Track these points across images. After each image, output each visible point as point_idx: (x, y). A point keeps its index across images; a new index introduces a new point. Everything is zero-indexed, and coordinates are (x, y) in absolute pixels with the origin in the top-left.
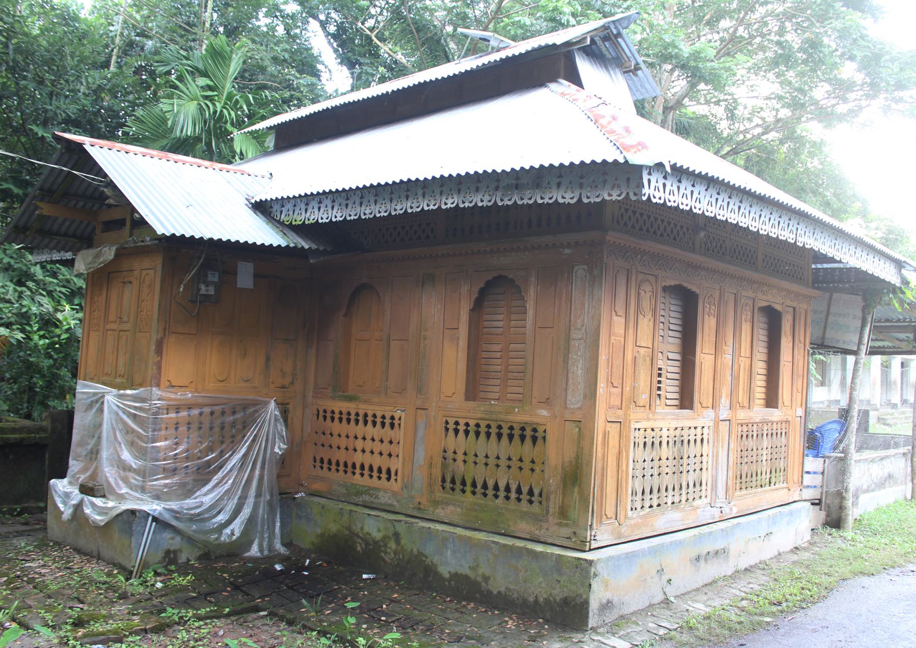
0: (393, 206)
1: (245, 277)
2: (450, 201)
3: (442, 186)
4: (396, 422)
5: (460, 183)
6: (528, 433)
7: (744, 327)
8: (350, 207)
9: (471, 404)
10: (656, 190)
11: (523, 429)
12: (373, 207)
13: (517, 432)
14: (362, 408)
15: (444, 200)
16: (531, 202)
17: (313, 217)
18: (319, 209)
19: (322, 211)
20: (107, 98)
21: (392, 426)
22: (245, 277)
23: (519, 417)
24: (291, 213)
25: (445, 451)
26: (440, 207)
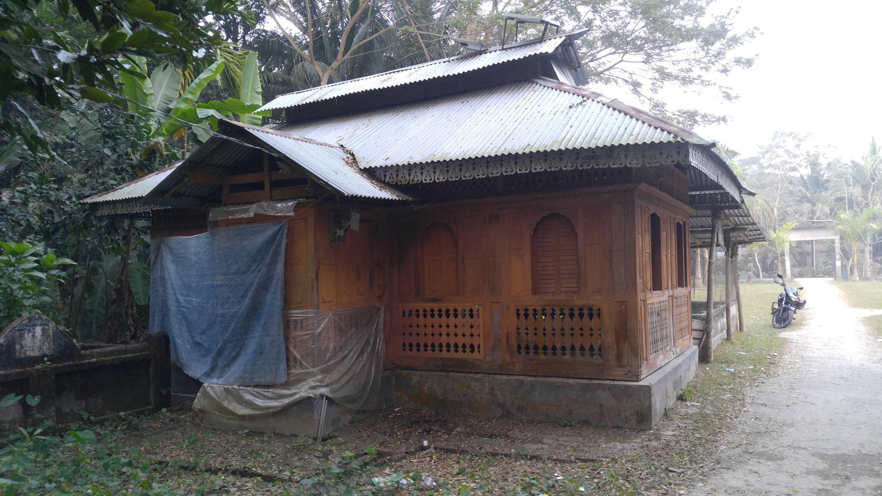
0: (463, 173)
1: (355, 222)
2: (495, 172)
3: (422, 169)
4: (475, 313)
5: (531, 157)
6: (586, 312)
7: (638, 228)
8: (450, 171)
9: (537, 297)
10: (695, 160)
11: (581, 309)
12: (471, 171)
13: (576, 312)
14: (444, 306)
15: (533, 166)
16: (605, 167)
17: (416, 179)
18: (422, 173)
19: (424, 174)
20: (334, 466)
21: (472, 316)
22: (355, 222)
23: (577, 301)
24: (395, 176)
25: (518, 329)
26: (609, 166)
